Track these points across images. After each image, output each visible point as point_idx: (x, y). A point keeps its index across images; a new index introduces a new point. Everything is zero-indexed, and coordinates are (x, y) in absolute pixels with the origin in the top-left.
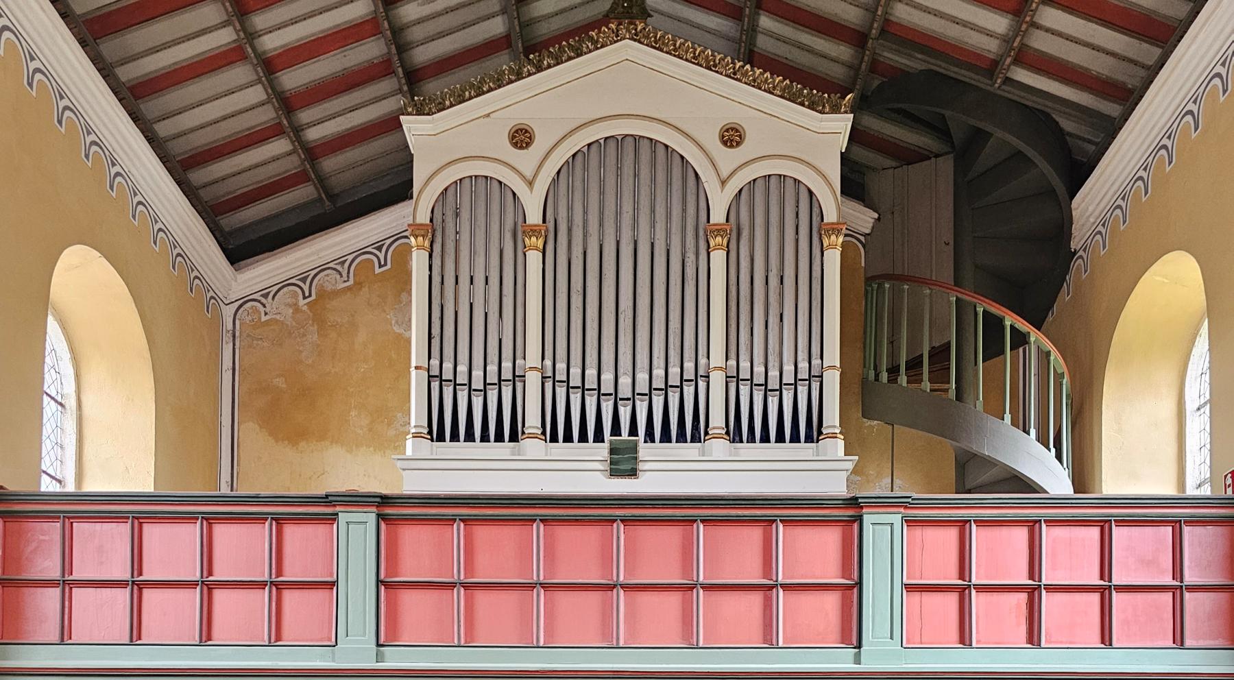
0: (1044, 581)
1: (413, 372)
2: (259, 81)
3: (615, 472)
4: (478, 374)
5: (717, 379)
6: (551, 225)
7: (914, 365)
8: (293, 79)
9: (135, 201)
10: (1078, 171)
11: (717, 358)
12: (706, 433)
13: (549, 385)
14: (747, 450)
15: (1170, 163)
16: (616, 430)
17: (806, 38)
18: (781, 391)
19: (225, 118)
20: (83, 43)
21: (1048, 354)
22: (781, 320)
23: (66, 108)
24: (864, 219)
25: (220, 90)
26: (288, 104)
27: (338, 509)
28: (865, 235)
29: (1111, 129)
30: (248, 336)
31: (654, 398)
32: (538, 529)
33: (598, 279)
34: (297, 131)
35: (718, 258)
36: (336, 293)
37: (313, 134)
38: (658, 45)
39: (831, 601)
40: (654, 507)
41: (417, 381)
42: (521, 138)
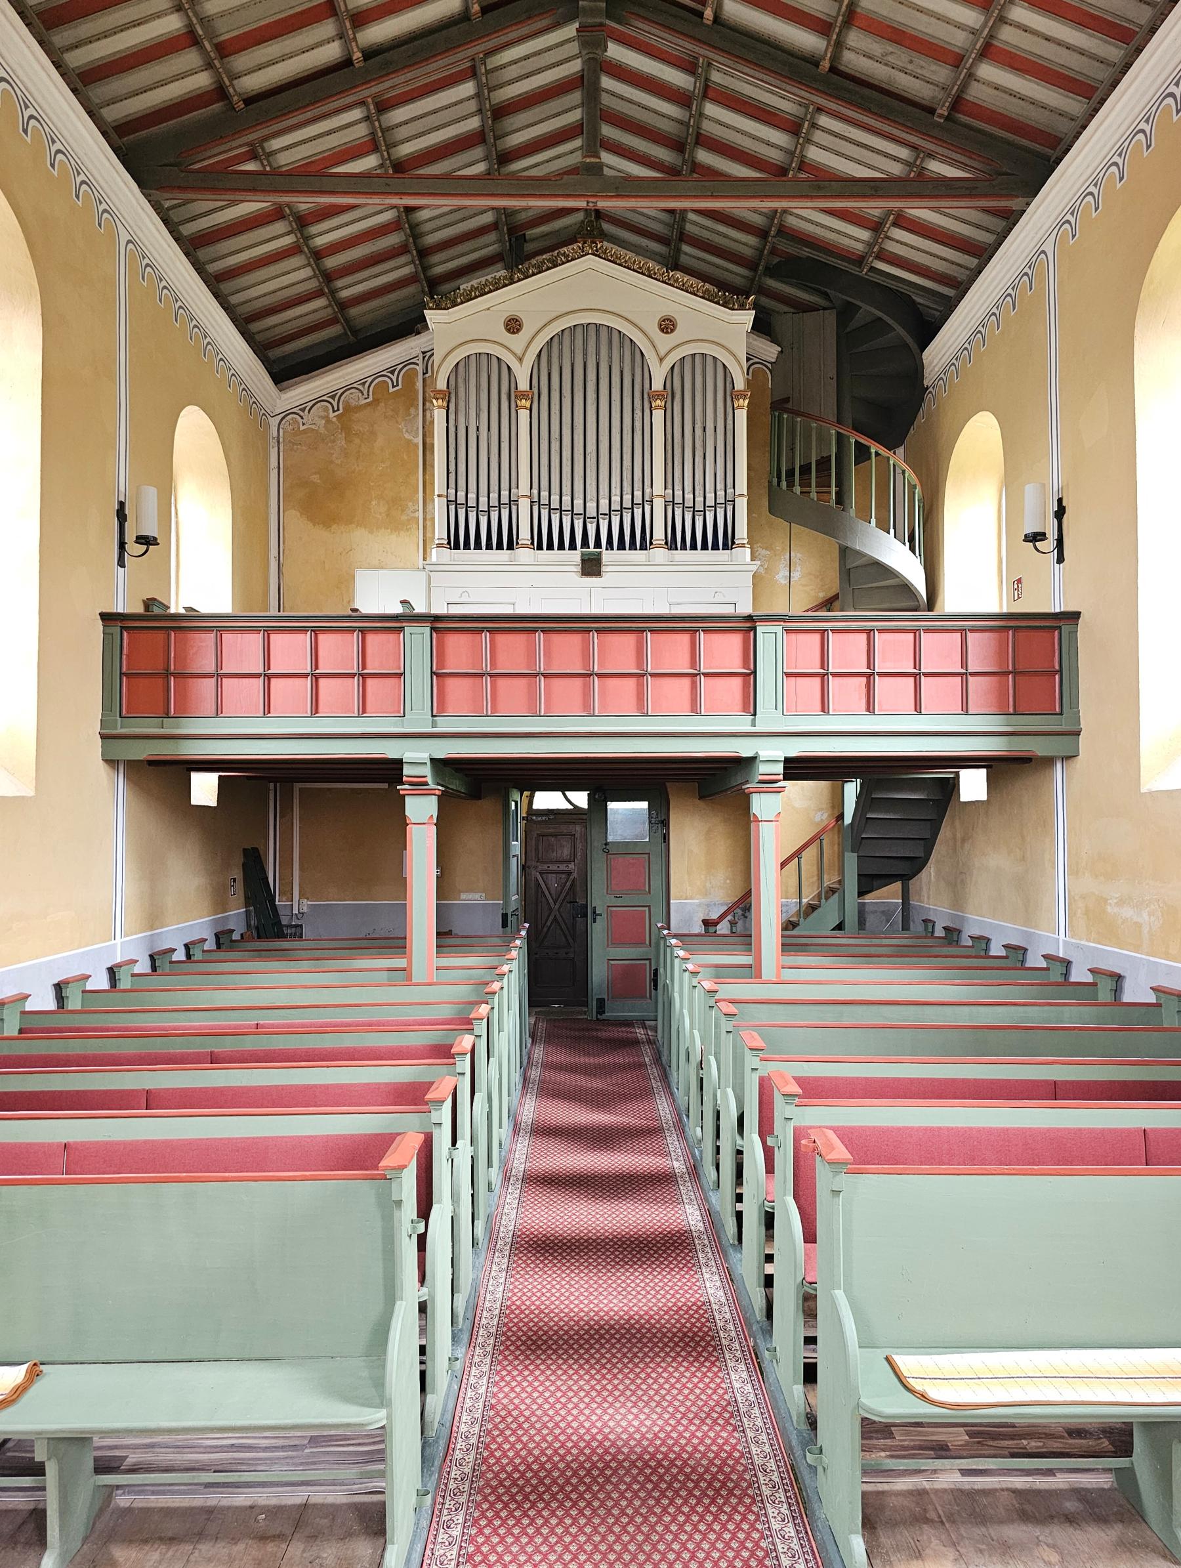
0: (877, 670)
1: (436, 499)
4: (483, 500)
5: (659, 504)
6: (535, 390)
7: (805, 470)
8: (331, 262)
9: (78, 180)
10: (927, 330)
11: (659, 488)
12: (651, 543)
13: (536, 508)
14: (679, 555)
16: (585, 543)
18: (705, 511)
19: (282, 289)
20: (187, 254)
23: (31, 117)
24: (770, 351)
26: (328, 277)
29: (950, 305)
31: (613, 518)
32: (540, 637)
34: (333, 292)
35: (658, 415)
36: (359, 408)
37: (344, 294)
39: (737, 682)
40: (617, 622)
41: (439, 508)
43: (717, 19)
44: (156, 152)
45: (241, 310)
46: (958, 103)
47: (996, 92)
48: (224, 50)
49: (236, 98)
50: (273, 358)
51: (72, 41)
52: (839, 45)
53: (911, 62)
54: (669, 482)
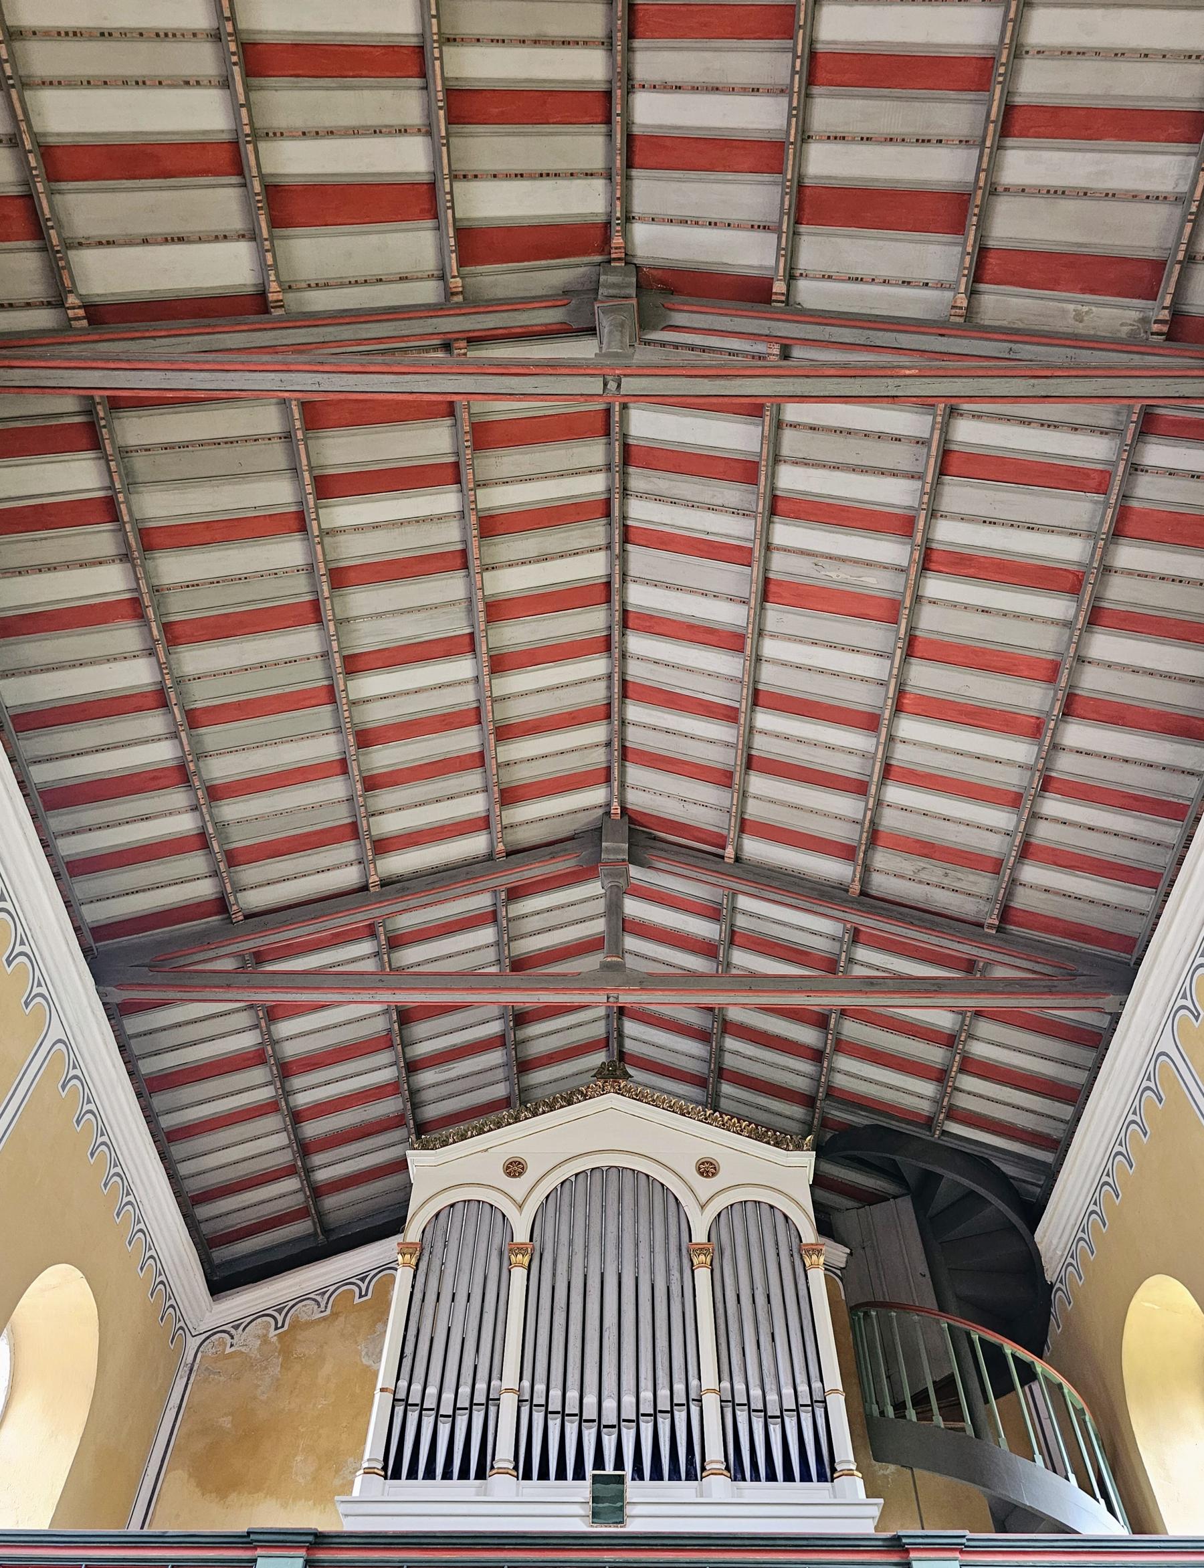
1: (378, 1394)
2: (285, 1129)
3: (615, 1469)
6: (537, 1244)
8: (313, 1129)
10: (1033, 1211)
11: (709, 1377)
12: (703, 1469)
15: (1117, 1196)
16: (599, 1462)
17: (763, 1100)
19: (245, 1160)
20: (139, 1095)
21: (1060, 1386)
22: (773, 1340)
24: (838, 1254)
25: (246, 1136)
26: (305, 1149)
27: (259, 1552)
28: (841, 1269)
29: (1051, 1174)
30: (207, 1369)
31: (642, 1425)
33: (582, 1296)
34: (308, 1171)
35: (703, 1275)
37: (321, 1176)
38: (639, 1098)
41: (380, 1405)
42: (515, 1168)
43: (738, 859)
44: (130, 960)
45: (205, 1229)
46: (1006, 914)
47: (1046, 895)
48: (233, 858)
49: (235, 908)
50: (217, 1261)
51: (70, 826)
52: (867, 869)
53: (946, 875)
54: (724, 1370)
